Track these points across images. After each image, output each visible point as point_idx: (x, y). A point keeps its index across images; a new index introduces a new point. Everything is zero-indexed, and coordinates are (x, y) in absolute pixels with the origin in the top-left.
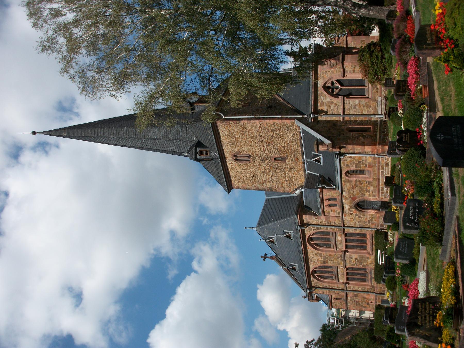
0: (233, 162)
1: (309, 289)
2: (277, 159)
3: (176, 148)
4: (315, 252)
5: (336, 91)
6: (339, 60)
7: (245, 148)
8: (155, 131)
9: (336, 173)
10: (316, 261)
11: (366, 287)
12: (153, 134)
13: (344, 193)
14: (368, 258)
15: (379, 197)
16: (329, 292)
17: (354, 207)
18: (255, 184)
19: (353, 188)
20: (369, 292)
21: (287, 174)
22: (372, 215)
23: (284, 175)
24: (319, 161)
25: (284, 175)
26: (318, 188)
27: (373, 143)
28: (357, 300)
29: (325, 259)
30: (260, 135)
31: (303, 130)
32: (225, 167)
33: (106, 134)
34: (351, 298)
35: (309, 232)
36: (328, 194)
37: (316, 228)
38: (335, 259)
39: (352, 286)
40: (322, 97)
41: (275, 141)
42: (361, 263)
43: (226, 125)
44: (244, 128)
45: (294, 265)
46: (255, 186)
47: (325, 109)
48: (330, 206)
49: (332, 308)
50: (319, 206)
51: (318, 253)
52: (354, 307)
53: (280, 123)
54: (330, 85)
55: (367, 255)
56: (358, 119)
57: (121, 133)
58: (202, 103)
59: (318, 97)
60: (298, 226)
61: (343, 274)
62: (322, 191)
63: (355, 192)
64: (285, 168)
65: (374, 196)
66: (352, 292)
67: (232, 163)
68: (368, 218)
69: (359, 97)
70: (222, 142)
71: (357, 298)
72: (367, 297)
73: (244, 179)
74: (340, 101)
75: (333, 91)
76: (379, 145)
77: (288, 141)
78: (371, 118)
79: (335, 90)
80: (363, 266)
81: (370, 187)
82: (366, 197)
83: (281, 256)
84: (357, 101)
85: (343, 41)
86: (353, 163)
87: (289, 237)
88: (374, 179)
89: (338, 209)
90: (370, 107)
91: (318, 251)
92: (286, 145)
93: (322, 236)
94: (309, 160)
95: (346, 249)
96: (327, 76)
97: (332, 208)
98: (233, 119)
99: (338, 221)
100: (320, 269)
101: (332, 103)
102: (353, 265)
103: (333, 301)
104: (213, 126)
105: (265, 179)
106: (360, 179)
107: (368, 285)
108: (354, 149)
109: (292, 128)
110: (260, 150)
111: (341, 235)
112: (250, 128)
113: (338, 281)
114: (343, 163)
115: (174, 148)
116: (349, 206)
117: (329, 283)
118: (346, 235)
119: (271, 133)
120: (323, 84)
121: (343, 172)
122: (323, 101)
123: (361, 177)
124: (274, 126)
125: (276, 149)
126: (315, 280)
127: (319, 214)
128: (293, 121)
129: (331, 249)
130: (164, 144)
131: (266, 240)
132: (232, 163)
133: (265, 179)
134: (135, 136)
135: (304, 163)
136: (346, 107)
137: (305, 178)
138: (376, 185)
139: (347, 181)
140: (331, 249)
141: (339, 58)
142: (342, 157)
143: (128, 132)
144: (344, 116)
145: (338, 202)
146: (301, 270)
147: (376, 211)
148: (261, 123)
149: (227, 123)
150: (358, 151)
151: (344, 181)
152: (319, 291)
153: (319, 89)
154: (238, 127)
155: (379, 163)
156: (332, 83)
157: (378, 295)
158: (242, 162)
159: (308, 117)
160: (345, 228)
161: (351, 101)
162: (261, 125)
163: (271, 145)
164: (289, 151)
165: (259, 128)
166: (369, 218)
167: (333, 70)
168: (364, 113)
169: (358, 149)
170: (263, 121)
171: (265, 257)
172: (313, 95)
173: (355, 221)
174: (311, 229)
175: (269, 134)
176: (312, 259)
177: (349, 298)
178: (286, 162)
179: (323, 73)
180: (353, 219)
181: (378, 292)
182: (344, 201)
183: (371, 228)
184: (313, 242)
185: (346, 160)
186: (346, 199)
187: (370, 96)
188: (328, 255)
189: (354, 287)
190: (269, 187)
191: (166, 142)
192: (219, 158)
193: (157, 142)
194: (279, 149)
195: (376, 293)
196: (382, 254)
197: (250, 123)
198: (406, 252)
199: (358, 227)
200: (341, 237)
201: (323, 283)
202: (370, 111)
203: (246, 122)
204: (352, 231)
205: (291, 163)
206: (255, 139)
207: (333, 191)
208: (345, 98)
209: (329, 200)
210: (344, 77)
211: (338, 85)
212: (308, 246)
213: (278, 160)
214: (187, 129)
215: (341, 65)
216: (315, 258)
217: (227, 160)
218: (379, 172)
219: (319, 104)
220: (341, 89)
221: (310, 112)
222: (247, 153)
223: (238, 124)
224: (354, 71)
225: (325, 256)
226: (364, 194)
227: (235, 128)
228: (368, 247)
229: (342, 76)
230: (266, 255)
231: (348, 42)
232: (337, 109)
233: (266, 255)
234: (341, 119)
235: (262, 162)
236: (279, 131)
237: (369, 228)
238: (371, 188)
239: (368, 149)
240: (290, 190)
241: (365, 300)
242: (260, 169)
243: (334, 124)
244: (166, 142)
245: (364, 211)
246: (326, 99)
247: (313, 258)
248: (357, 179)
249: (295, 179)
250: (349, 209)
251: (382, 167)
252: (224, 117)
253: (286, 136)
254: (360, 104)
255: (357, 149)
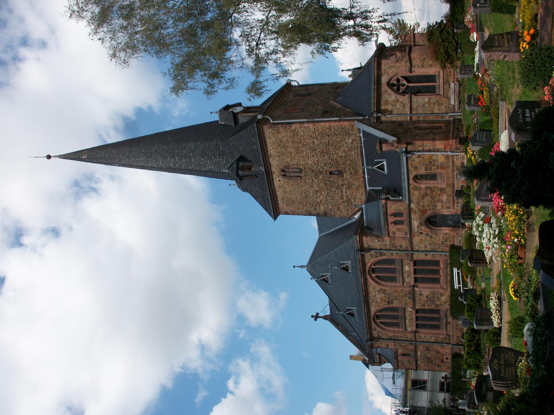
0: (281, 179)
1: (370, 340)
2: (333, 172)
3: (215, 167)
4: (378, 287)
5: (402, 89)
6: (405, 52)
7: (296, 161)
8: (191, 147)
9: (403, 177)
10: (379, 300)
11: (440, 336)
12: (189, 151)
13: (412, 205)
14: (442, 295)
15: (454, 208)
16: (394, 345)
17: (424, 224)
18: (306, 207)
19: (423, 197)
20: (443, 343)
21: (344, 193)
22: (446, 234)
23: (341, 194)
24: (382, 168)
25: (341, 194)
26: (382, 199)
27: (446, 138)
28: (429, 356)
29: (389, 298)
30: (313, 142)
31: (364, 132)
32: (271, 185)
33: (133, 154)
34: (421, 353)
35: (370, 260)
36: (393, 207)
37: (378, 255)
38: (402, 297)
39: (423, 336)
40: (386, 95)
41: (331, 150)
42: (433, 302)
43: (275, 130)
44: (295, 133)
45: (351, 310)
46: (307, 210)
47: (390, 108)
48: (395, 223)
49: (398, 368)
50: (382, 223)
51: (381, 289)
52: (425, 366)
53: (337, 126)
54: (395, 82)
55: (441, 291)
56: (428, 118)
57: (151, 151)
58: (247, 112)
59: (381, 95)
60: (357, 251)
61: (411, 319)
62: (386, 204)
63: (426, 204)
64: (343, 185)
65: (448, 208)
66: (422, 344)
67: (279, 181)
68: (441, 238)
69: (429, 94)
70: (269, 154)
71: (429, 354)
72: (441, 351)
73: (293, 202)
74: (407, 99)
75: (398, 89)
76: (453, 138)
77: (347, 149)
78: (443, 117)
79: (401, 87)
80: (437, 306)
81: (442, 196)
82: (439, 210)
83: (336, 299)
84: (426, 99)
85: (411, 38)
86: (423, 164)
87: (346, 269)
88: (447, 184)
89: (405, 227)
90: (442, 104)
91: (381, 287)
92: (344, 155)
93: (386, 266)
94: (370, 167)
95: (416, 284)
96: (391, 71)
97: (398, 227)
98: (282, 123)
99: (405, 244)
100: (384, 313)
101: (397, 101)
102: (424, 305)
103: (399, 358)
104: (259, 132)
105: (319, 200)
106: (431, 186)
107: (442, 334)
108: (423, 145)
109: (351, 132)
110: (313, 162)
111: (408, 264)
112: (302, 134)
113: (406, 329)
114: (411, 164)
115: (213, 167)
116: (418, 223)
117: (394, 332)
118: (415, 263)
119: (326, 139)
120: (387, 80)
121: (411, 177)
122: (388, 99)
123: (431, 183)
124: (331, 130)
125: (332, 160)
126: (378, 329)
127: (382, 235)
128: (352, 123)
129: (397, 284)
130: (201, 163)
131: (318, 278)
132: (279, 181)
133: (319, 200)
134: (167, 154)
135: (364, 178)
136: (414, 105)
137: (365, 197)
138: (449, 193)
139: (416, 188)
140: (397, 284)
142: (409, 155)
143: (159, 150)
144: (411, 115)
145: (405, 218)
146: (359, 314)
147: (451, 229)
148: (315, 127)
149: (276, 129)
150: (428, 148)
151: (412, 189)
152: (382, 344)
153: (383, 86)
154: (288, 132)
155: (453, 162)
156: (398, 80)
157: (455, 347)
158: (292, 178)
159: (370, 118)
160: (414, 253)
161: (419, 99)
162: (315, 129)
163: (326, 155)
164: (348, 162)
165: (312, 134)
166: (443, 239)
167: (398, 64)
168: (435, 112)
169: (428, 145)
170: (317, 124)
171: (316, 317)
172: (376, 92)
173: (426, 242)
174: (372, 256)
175: (324, 141)
176: (374, 298)
177: (419, 353)
178: (343, 177)
179: (387, 68)
180: (424, 240)
181: (455, 343)
182: (412, 216)
183: (445, 252)
184: (375, 275)
185: (414, 161)
186: (415, 212)
187: (442, 93)
188: (393, 291)
189: (425, 337)
190: (323, 210)
191: (203, 159)
192: (265, 173)
193: (193, 159)
194: (336, 160)
195: (452, 345)
196: (458, 273)
197: (302, 127)
198: (484, 141)
199: (429, 251)
200: (409, 267)
201: (387, 333)
202: (442, 110)
203: (297, 126)
204: (421, 256)
205: (350, 178)
206: (308, 147)
207: (399, 203)
208: (413, 95)
209: (395, 215)
210: (411, 72)
211: (404, 82)
212: (370, 280)
213: (335, 174)
214: (229, 142)
215: (407, 57)
216: (378, 296)
217: (275, 176)
218: (453, 175)
219: (382, 103)
220: (408, 86)
221: (372, 111)
222: (298, 166)
223: (288, 129)
224: (422, 65)
225: (389, 294)
226: (435, 206)
227: (284, 135)
228: (442, 279)
229: (408, 71)
230: (318, 314)
231: (416, 40)
232: (404, 107)
233: (318, 314)
234: (408, 119)
235: (315, 178)
236: (336, 136)
237: (443, 252)
238: (445, 198)
239: (439, 144)
240: (348, 214)
241: (439, 355)
242: (313, 188)
243: (400, 124)
244: (203, 159)
245: (436, 228)
246: (390, 97)
247: (375, 296)
248: (428, 186)
249: (354, 199)
250: (418, 227)
251: (456, 168)
252: (272, 122)
253: (344, 142)
254: (429, 102)
255: (426, 146)
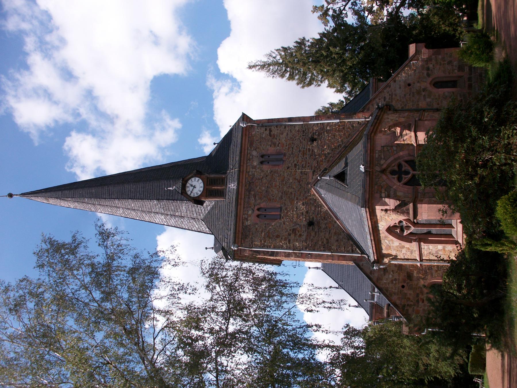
85: (411, 137)
141: (408, 209)
208: (422, 243)
